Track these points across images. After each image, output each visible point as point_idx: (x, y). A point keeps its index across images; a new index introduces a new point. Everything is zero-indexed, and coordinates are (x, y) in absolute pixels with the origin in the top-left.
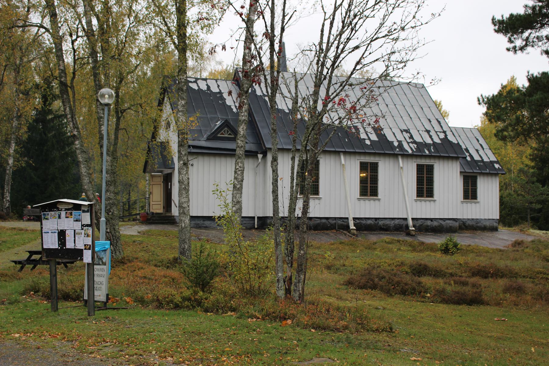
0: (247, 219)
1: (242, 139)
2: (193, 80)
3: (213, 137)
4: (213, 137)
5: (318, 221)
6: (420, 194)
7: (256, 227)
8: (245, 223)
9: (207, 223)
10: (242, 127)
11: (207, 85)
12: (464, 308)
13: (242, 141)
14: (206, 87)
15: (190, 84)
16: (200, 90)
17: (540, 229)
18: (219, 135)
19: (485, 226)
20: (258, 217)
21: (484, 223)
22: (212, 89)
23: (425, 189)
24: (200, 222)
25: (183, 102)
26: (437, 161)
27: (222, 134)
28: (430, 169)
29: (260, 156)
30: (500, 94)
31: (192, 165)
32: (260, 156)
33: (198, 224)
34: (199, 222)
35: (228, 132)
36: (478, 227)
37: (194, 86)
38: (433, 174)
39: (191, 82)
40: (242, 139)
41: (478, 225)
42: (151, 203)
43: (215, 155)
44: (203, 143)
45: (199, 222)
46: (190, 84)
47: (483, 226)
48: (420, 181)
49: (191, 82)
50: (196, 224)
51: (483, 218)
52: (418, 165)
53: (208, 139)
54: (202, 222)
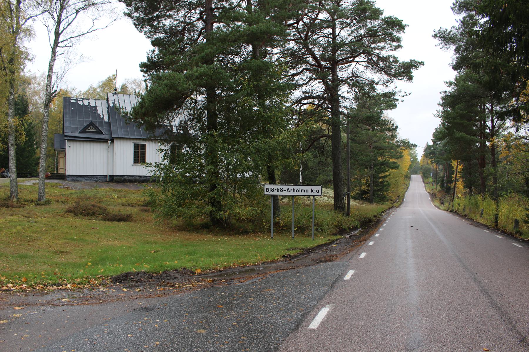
2: (80, 100)
3: (83, 131)
4: (83, 131)
5: (146, 178)
6: (136, 161)
9: (79, 179)
11: (89, 103)
12: (115, 224)
15: (79, 102)
23: (140, 159)
24: (75, 178)
25: (11, 111)
26: (147, 142)
28: (144, 147)
29: (109, 142)
30: (445, 116)
32: (109, 142)
37: (81, 103)
38: (145, 150)
43: (86, 141)
44: (77, 135)
46: (79, 102)
48: (136, 154)
52: (134, 144)
53: (80, 132)
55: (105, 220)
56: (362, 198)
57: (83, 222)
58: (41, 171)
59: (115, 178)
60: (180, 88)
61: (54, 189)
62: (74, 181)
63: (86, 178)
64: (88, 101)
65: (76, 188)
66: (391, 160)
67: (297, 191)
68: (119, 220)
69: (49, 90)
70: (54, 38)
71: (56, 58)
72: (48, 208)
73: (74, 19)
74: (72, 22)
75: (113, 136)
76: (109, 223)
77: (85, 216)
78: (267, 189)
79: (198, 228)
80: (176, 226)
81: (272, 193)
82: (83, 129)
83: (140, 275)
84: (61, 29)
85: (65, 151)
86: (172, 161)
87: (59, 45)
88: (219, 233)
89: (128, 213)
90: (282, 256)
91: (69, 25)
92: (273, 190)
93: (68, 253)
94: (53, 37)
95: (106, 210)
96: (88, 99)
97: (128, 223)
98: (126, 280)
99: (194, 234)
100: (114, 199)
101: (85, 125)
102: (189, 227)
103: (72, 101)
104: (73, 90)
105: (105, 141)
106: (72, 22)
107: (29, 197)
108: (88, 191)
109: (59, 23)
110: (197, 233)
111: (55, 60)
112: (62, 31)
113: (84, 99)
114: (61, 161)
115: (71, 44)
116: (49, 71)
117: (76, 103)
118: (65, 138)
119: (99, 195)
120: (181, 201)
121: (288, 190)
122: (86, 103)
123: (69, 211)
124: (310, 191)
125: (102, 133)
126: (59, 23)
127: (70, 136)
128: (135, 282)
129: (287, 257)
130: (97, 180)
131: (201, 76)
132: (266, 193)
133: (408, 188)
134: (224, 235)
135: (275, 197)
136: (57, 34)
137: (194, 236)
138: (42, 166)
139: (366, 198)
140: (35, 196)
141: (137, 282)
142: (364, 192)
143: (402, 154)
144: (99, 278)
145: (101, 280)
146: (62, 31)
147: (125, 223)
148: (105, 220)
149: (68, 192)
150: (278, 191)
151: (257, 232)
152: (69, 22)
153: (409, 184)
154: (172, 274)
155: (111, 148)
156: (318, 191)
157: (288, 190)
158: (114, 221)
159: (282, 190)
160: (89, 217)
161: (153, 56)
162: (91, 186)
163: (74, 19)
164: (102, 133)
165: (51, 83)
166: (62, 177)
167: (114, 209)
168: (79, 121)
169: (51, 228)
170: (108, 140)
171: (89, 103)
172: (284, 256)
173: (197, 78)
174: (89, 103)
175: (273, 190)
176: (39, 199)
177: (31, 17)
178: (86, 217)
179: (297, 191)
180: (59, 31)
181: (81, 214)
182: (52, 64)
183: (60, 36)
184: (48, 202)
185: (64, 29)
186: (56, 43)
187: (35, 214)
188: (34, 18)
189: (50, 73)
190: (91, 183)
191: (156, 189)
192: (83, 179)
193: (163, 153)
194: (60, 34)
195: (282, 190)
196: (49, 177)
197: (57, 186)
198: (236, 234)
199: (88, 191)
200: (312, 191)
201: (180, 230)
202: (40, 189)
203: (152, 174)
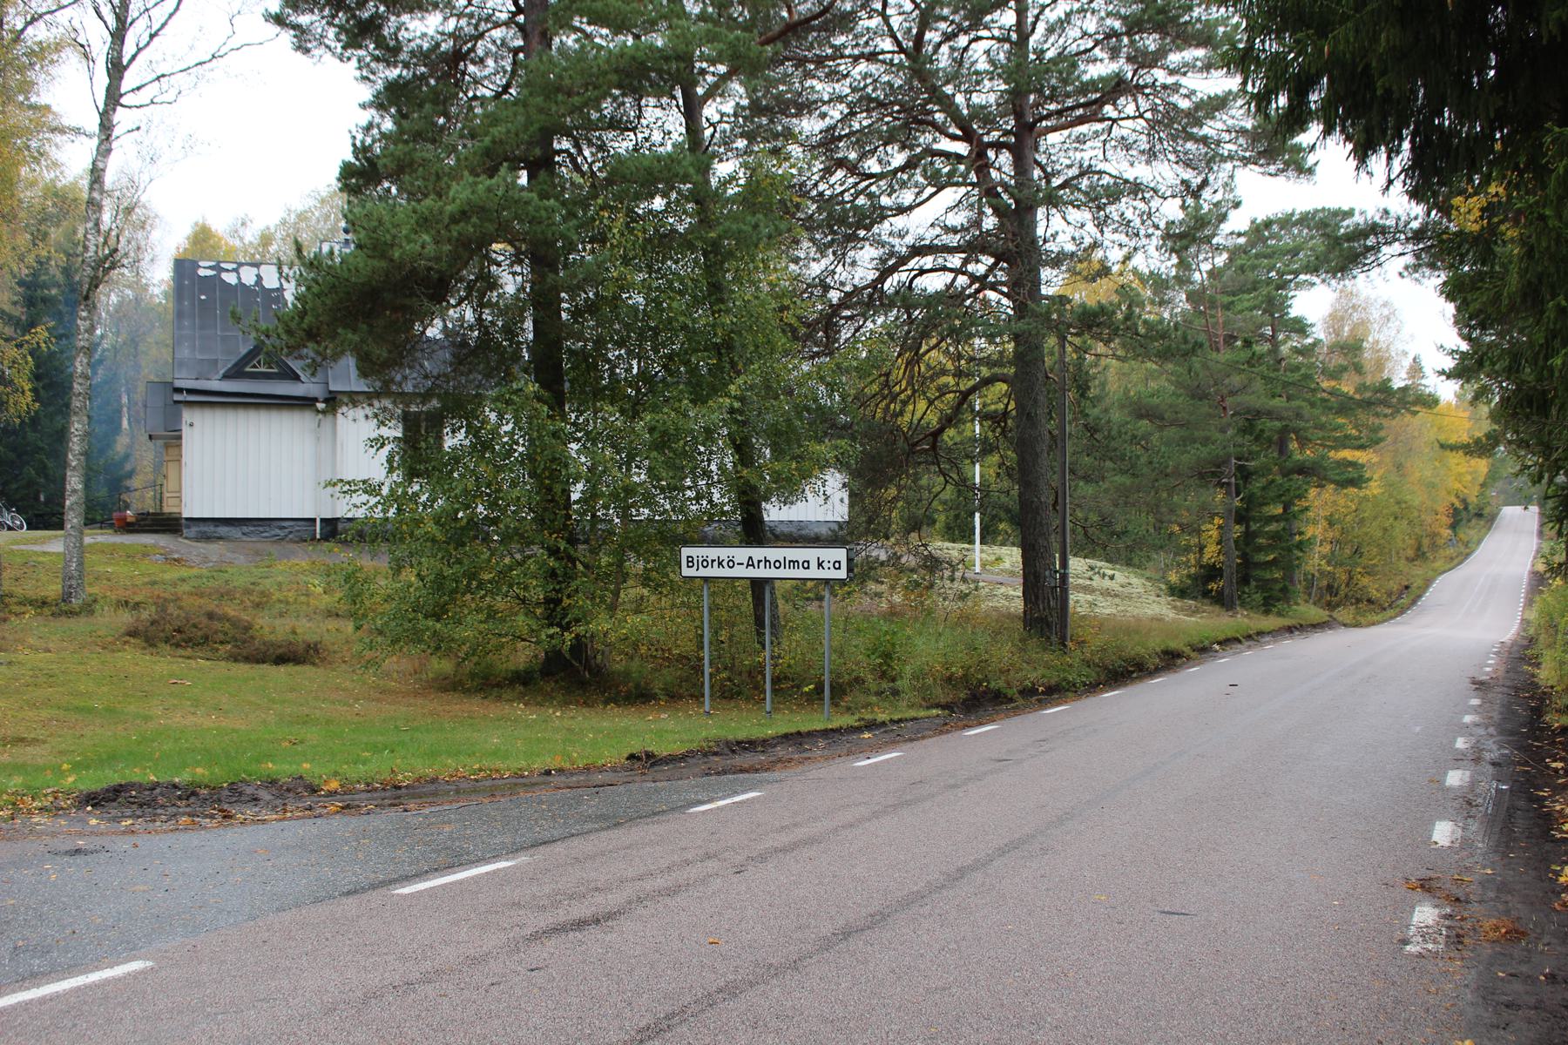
3: (236, 373)
4: (236, 373)
9: (223, 530)
11: (258, 276)
24: (210, 529)
37: (230, 278)
46: (224, 276)
53: (226, 377)
54: (212, 528)
55: (236, 660)
56: (1206, 594)
57: (164, 664)
58: (71, 509)
59: (340, 526)
60: (397, 255)
61: (121, 564)
62: (207, 538)
63: (245, 529)
64: (255, 271)
65: (206, 559)
66: (1332, 454)
67: (777, 564)
68: (280, 660)
69: (92, 248)
70: (107, 81)
71: (115, 145)
72: (79, 625)
73: (171, 15)
74: (163, 26)
75: (332, 388)
76: (243, 669)
77: (178, 645)
78: (690, 560)
81: (703, 572)
83: (158, 791)
84: (129, 49)
85: (180, 438)
86: (411, 474)
87: (123, 101)
88: (553, 698)
91: (152, 36)
92: (706, 563)
94: (102, 80)
95: (248, 628)
96: (257, 265)
97: (307, 669)
99: (477, 700)
100: (302, 591)
101: (244, 351)
102: (486, 683)
103: (202, 272)
104: (243, 224)
106: (163, 26)
107: (28, 589)
108: (236, 565)
109: (118, 36)
110: (499, 698)
111: (109, 151)
112: (134, 57)
113: (241, 265)
114: (172, 474)
115: (170, 97)
116: (91, 189)
117: (218, 277)
118: (177, 397)
119: (267, 584)
120: (441, 601)
121: (750, 563)
123: (133, 633)
124: (814, 564)
125: (297, 378)
126: (118, 36)
128: (135, 807)
129: (639, 759)
130: (282, 533)
131: (463, 213)
132: (686, 572)
133: (1468, 555)
134: (565, 704)
135: (758, 585)
136: (117, 69)
137: (474, 705)
138: (74, 491)
139: (1220, 593)
140: (53, 590)
141: (141, 806)
142: (1212, 572)
143: (1382, 434)
146: (134, 57)
147: (298, 668)
148: (235, 659)
149: (172, 574)
150: (720, 564)
151: (681, 697)
152: (156, 27)
153: (1479, 542)
156: (837, 565)
157: (750, 563)
159: (732, 563)
160: (189, 652)
161: (369, 141)
163: (171, 15)
166: (168, 524)
170: (316, 400)
171: (259, 278)
173: (454, 220)
174: (259, 278)
175: (706, 563)
176: (66, 597)
177: (41, 16)
178: (181, 652)
179: (777, 564)
180: (120, 56)
181: (167, 641)
182: (101, 165)
183: (127, 74)
184: (88, 608)
185: (139, 50)
186: (114, 97)
187: (22, 641)
188: (47, 17)
189: (96, 195)
190: (259, 546)
193: (387, 448)
194: (126, 68)
195: (732, 563)
197: (145, 555)
200: (820, 565)
202: (67, 566)
203: (360, 513)
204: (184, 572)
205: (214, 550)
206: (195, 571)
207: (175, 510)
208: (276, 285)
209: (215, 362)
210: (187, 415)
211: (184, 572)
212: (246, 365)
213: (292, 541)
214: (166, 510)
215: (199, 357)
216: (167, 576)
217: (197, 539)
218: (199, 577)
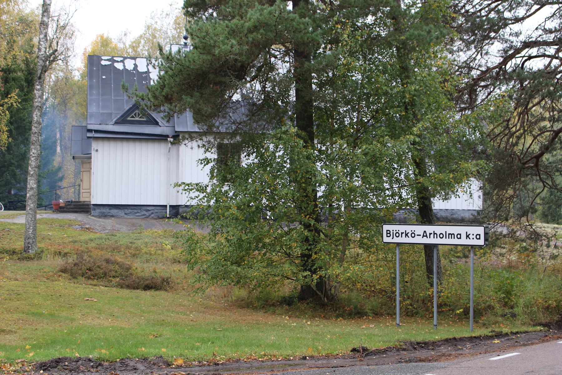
0: (158, 208)
1: (36, 125)
3: (122, 121)
4: (122, 121)
7: (168, 216)
8: (157, 212)
9: (114, 211)
10: (35, 113)
13: (36, 127)
14: (134, 66)
15: (116, 65)
16: (125, 69)
17: (548, 223)
18: (129, 119)
19: (462, 217)
20: (170, 206)
21: (462, 215)
22: (138, 69)
24: (106, 211)
27: (133, 117)
31: (97, 151)
33: (104, 213)
34: (104, 211)
35: (139, 115)
36: (453, 219)
37: (119, 66)
39: (118, 62)
40: (36, 125)
41: (454, 216)
42: (82, 191)
43: (153, 140)
44: (111, 128)
45: (104, 211)
46: (116, 65)
47: (460, 218)
49: (118, 62)
50: (101, 212)
51: (460, 209)
53: (116, 123)
54: (108, 210)
57: (81, 289)
58: (30, 198)
59: (181, 210)
60: (217, 52)
61: (58, 230)
64: (133, 61)
65: (104, 229)
67: (441, 236)
68: (147, 288)
69: (43, 50)
72: (33, 265)
75: (177, 129)
76: (126, 292)
77: (89, 278)
79: (273, 305)
80: (237, 301)
81: (396, 240)
82: (122, 116)
83: (80, 362)
86: (224, 180)
89: (165, 275)
90: (350, 349)
92: (398, 234)
93: (10, 332)
96: (134, 58)
97: (162, 293)
98: (56, 367)
100: (159, 249)
101: (127, 108)
103: (103, 63)
104: (125, 35)
105: (162, 138)
110: (274, 313)
117: (112, 66)
119: (139, 243)
120: (240, 254)
121: (425, 235)
122: (129, 64)
124: (464, 236)
125: (157, 123)
127: (97, 131)
131: (255, 27)
132: (386, 239)
134: (313, 317)
137: (260, 316)
138: (32, 188)
140: (19, 245)
144: (17, 363)
145: (20, 365)
149: (86, 236)
150: (406, 235)
151: (382, 315)
154: (132, 364)
155: (175, 148)
158: (138, 289)
159: (413, 235)
160: (95, 282)
162: (133, 225)
164: (157, 123)
165: (46, 36)
166: (83, 208)
167: (142, 268)
168: (115, 101)
169: (14, 296)
170: (167, 136)
171: (136, 66)
172: (354, 350)
173: (250, 31)
174: (136, 66)
176: (26, 249)
178: (90, 282)
179: (441, 236)
184: (39, 256)
189: (45, 19)
190: (134, 221)
191: (201, 231)
192: (121, 213)
195: (413, 235)
196: (61, 208)
197: (70, 225)
198: (337, 317)
199: (121, 231)
200: (467, 236)
201: (242, 307)
203: (194, 203)
204: (92, 236)
205: (109, 223)
206: (98, 235)
207: (87, 200)
208: (146, 70)
209: (111, 113)
210: (95, 145)
211: (92, 236)
212: (128, 116)
213: (153, 218)
214: (82, 199)
215: (101, 111)
216: (82, 238)
217: (100, 217)
218: (101, 238)
